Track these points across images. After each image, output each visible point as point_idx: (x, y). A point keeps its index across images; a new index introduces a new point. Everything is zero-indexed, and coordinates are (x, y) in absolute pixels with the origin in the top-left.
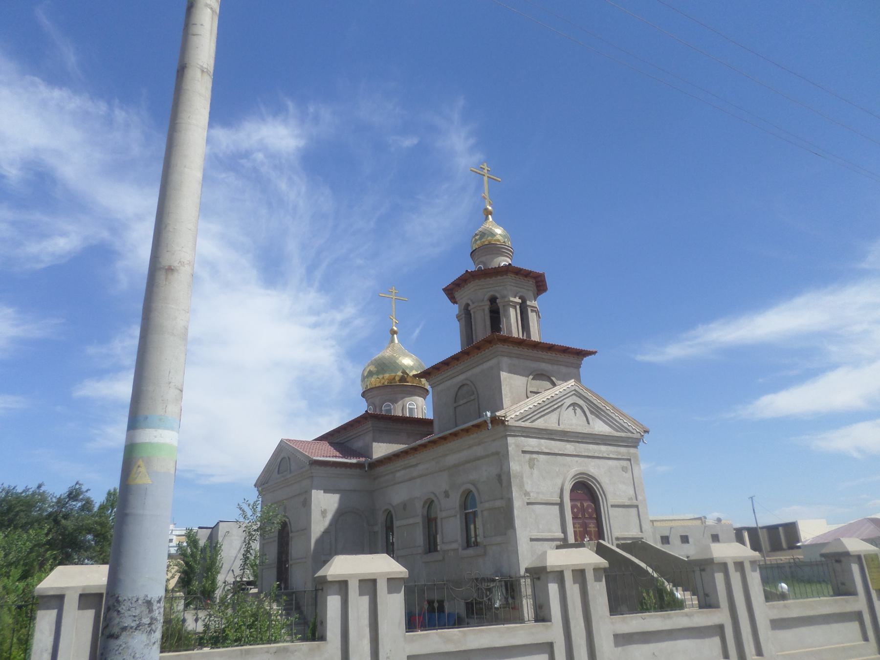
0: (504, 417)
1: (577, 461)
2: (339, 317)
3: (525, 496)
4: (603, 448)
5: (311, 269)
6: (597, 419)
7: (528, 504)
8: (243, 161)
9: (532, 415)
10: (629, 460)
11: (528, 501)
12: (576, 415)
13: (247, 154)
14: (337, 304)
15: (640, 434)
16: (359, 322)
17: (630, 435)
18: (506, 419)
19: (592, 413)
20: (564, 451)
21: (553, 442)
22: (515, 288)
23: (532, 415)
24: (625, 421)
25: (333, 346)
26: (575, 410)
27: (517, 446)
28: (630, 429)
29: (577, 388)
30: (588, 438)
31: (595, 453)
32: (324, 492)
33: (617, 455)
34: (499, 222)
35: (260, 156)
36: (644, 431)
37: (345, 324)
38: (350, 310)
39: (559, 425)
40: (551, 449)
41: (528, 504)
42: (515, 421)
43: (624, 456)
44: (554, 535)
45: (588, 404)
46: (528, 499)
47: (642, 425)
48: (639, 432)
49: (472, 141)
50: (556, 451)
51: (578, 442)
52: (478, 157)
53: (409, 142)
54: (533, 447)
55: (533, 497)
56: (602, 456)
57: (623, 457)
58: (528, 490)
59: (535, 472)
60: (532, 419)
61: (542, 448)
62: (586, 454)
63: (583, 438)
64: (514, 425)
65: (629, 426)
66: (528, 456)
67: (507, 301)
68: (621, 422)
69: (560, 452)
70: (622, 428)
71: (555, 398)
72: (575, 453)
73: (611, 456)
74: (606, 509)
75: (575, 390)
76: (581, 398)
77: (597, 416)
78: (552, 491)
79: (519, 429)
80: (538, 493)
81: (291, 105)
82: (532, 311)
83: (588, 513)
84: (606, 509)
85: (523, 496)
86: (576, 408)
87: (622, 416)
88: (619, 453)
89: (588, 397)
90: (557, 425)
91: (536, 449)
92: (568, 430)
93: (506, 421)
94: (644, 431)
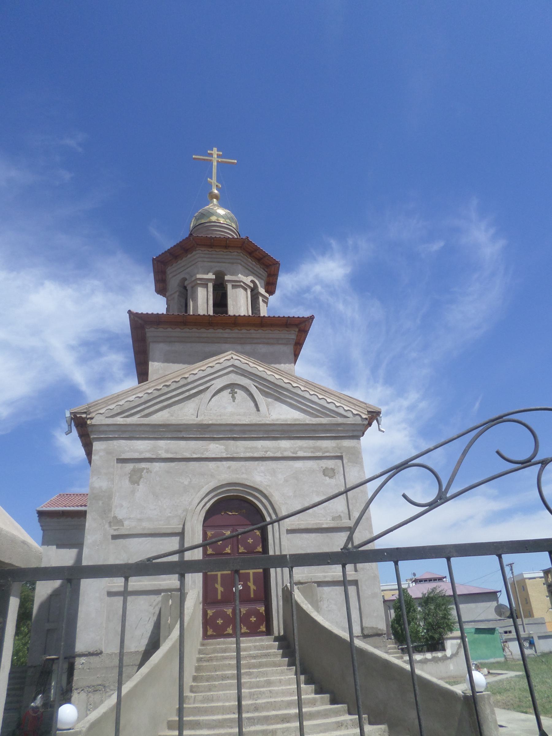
0: (85, 413)
1: (229, 467)
2: (406, 403)
3: (110, 526)
4: (285, 444)
5: (374, 369)
6: (276, 402)
7: (115, 537)
8: (306, 295)
9: (143, 406)
10: (341, 458)
11: (115, 533)
12: (234, 401)
13: (308, 289)
14: (401, 392)
15: (360, 416)
16: (423, 405)
17: (340, 420)
18: (88, 416)
19: (266, 394)
20: (202, 454)
21: (183, 443)
22: (209, 264)
23: (143, 406)
24: (329, 400)
25: (405, 429)
26: (233, 393)
27: (109, 453)
28: (341, 411)
29: (237, 363)
30: (255, 431)
31: (266, 452)
32: (57, 548)
33: (312, 452)
34: (223, 205)
35: (318, 288)
36: (368, 412)
37: (411, 408)
38: (413, 396)
39: (197, 417)
40: (176, 453)
41: (115, 537)
42: (107, 417)
43: (327, 452)
44: (160, 585)
45: (260, 384)
46: (115, 530)
47: (366, 404)
48: (357, 414)
49: (492, 231)
50: (187, 455)
51: (234, 439)
52: (501, 243)
53: (437, 246)
54: (141, 453)
55: (128, 526)
56: (280, 456)
57: (327, 454)
58: (120, 517)
59: (142, 488)
60: (143, 413)
61: (160, 452)
62: (248, 455)
63: (244, 432)
64: (103, 423)
65: (337, 407)
66: (130, 466)
67: (194, 281)
68: (323, 402)
69: (195, 456)
70: (325, 411)
71: (189, 380)
72: (224, 455)
73: (300, 454)
74: (277, 535)
75: (233, 366)
76: (245, 376)
77: (278, 399)
78: (169, 514)
79: (111, 428)
80: (140, 520)
81: (334, 243)
82: (234, 287)
83: (246, 545)
84: (277, 535)
85: (107, 526)
86: (236, 390)
87: (323, 393)
88: (319, 449)
89: (259, 373)
90: (194, 417)
91: (148, 455)
92: (210, 422)
93: (88, 419)
94: (368, 412)
